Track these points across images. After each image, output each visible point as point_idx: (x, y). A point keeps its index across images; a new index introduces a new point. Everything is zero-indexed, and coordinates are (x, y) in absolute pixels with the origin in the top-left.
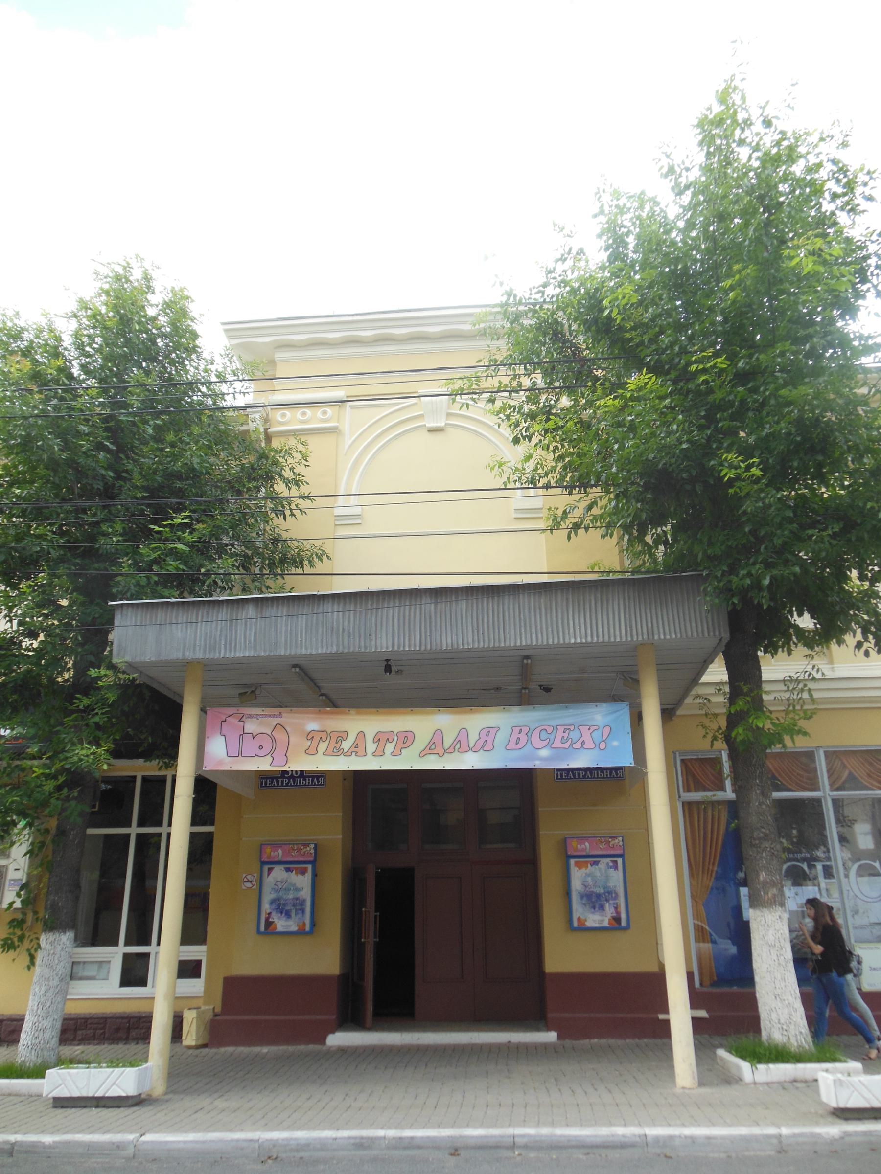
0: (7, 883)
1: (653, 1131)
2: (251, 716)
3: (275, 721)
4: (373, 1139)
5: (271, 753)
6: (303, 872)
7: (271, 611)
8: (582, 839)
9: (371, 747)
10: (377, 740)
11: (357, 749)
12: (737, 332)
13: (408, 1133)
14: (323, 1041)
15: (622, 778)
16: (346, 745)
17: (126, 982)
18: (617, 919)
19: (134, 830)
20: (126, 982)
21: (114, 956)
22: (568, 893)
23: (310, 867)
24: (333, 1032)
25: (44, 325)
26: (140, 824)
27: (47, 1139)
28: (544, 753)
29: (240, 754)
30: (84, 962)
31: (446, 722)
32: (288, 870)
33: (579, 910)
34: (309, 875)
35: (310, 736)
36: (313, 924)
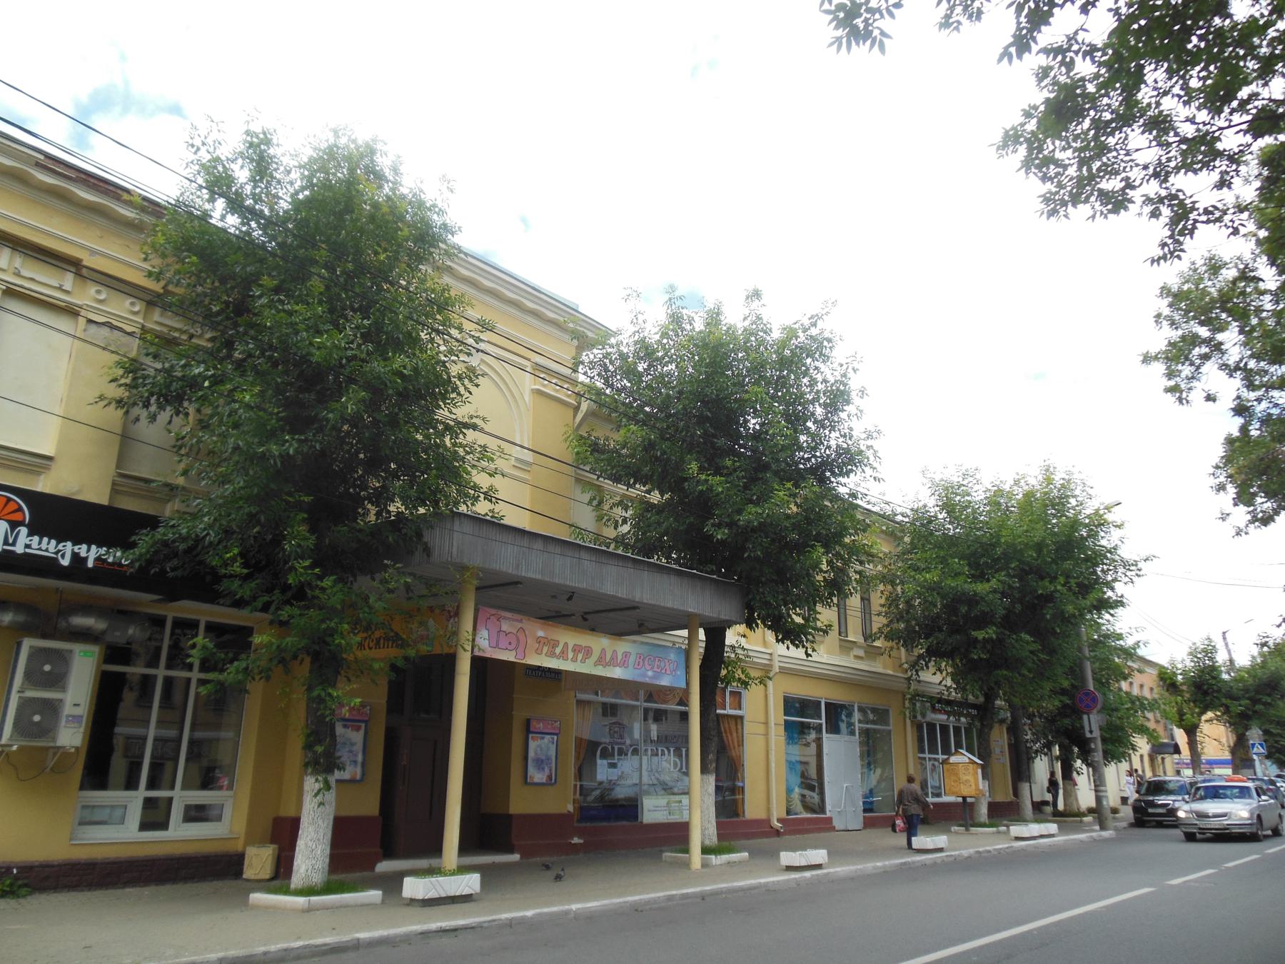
0: (64, 720)
1: (762, 881)
2: (505, 618)
3: (520, 625)
4: (673, 896)
5: (516, 649)
6: (358, 729)
7: (551, 548)
8: (539, 721)
9: (571, 655)
10: (574, 651)
11: (563, 656)
12: (1205, 651)
13: (685, 891)
14: (372, 868)
15: (560, 680)
16: (558, 651)
17: (144, 826)
18: (550, 777)
19: (161, 673)
20: (144, 826)
21: (134, 801)
22: (526, 758)
23: (363, 725)
24: (381, 861)
25: (933, 511)
26: (168, 667)
27: (529, 913)
28: (650, 673)
29: (497, 646)
30: (94, 807)
31: (600, 643)
32: (345, 726)
33: (532, 770)
34: (362, 732)
35: (539, 640)
36: (363, 774)
